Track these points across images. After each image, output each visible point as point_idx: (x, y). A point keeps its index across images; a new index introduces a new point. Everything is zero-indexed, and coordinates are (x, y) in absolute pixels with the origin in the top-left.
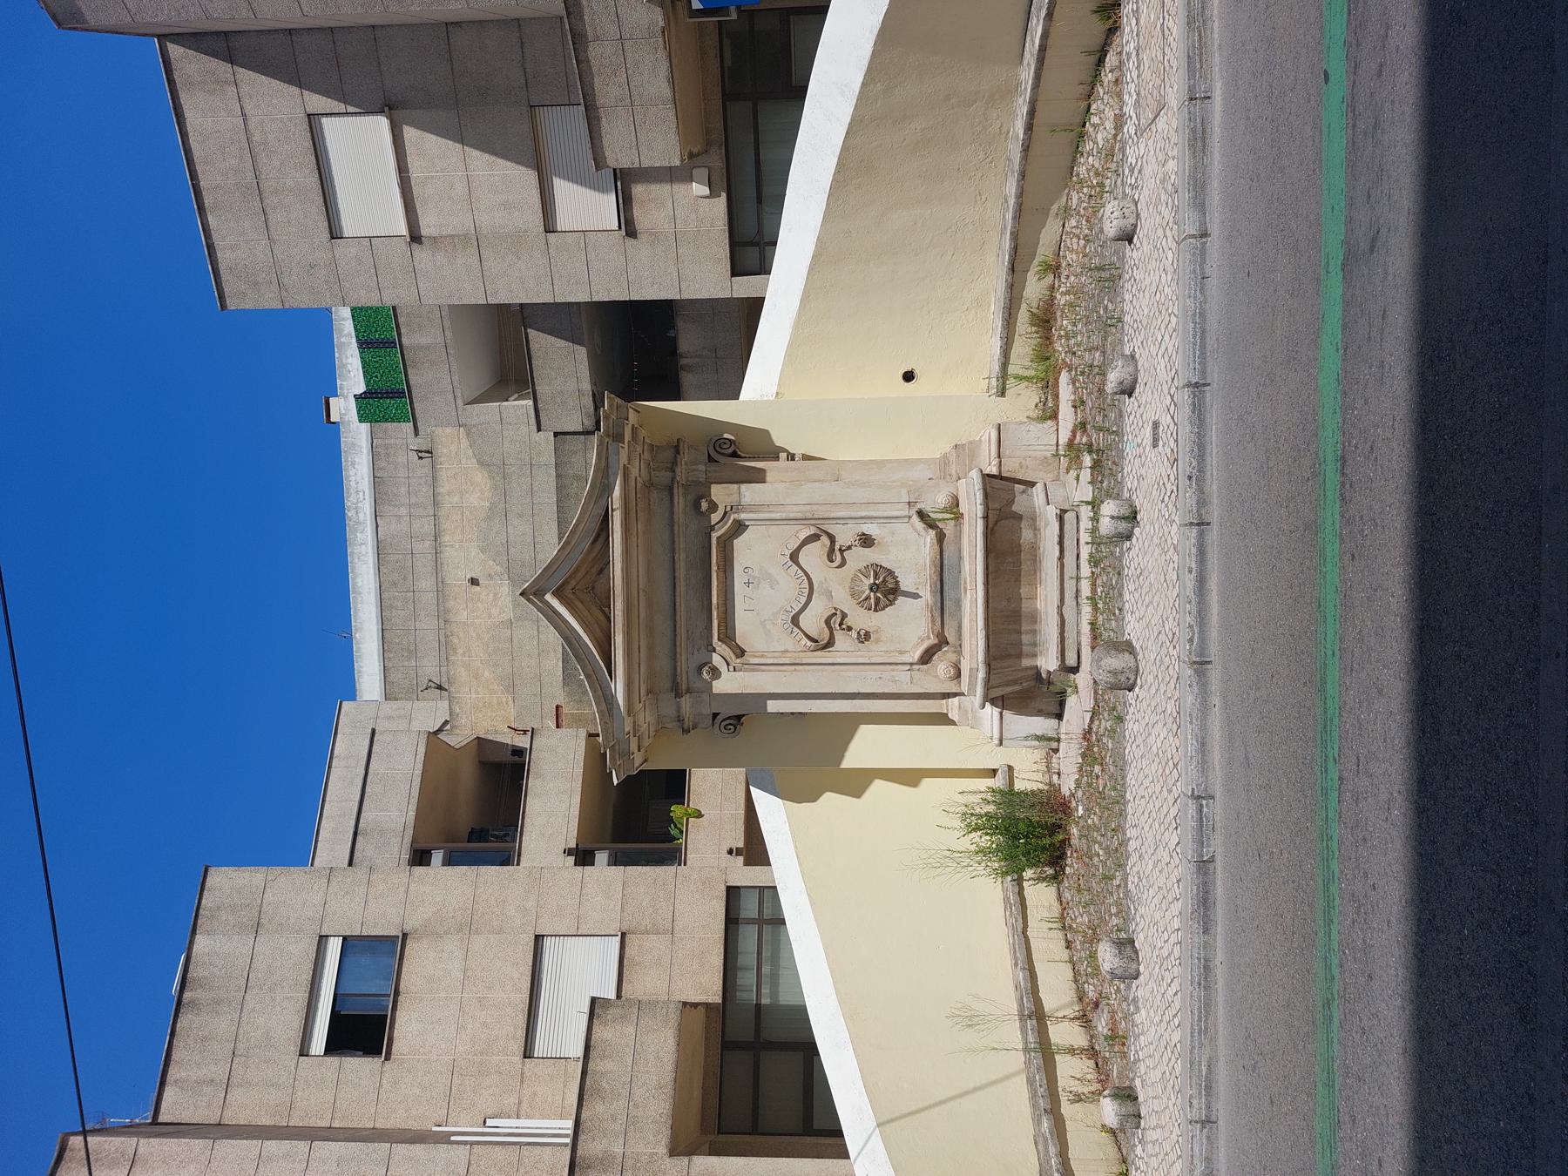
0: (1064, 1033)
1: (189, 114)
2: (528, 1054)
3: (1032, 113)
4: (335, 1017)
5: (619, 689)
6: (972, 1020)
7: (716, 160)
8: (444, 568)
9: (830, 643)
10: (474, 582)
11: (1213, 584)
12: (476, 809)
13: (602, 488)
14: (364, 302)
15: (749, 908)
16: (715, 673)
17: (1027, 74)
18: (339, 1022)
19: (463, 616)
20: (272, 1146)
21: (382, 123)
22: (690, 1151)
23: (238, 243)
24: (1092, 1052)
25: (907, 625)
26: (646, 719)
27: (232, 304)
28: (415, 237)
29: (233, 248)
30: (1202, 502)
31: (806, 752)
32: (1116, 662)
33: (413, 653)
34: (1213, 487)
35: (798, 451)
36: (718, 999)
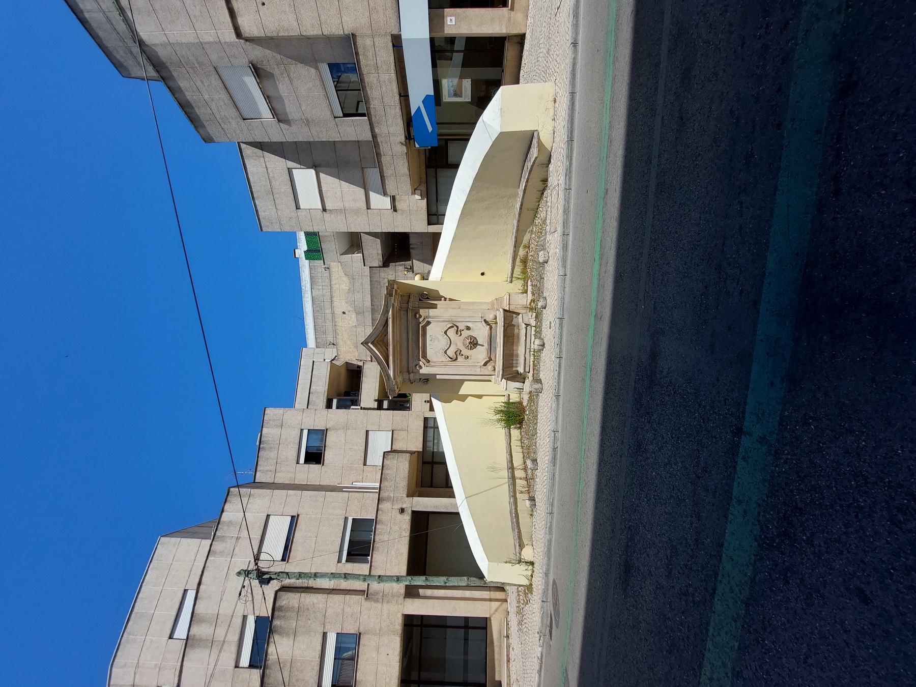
0: (519, 473)
1: (248, 167)
2: (365, 464)
3: (522, 205)
4: (307, 453)
5: (391, 373)
6: (493, 469)
7: (423, 188)
8: (336, 311)
9: (456, 359)
10: (344, 313)
11: (562, 374)
12: (346, 388)
13: (386, 312)
14: (308, 230)
15: (431, 424)
16: (421, 367)
17: (521, 194)
18: (308, 455)
20: (290, 492)
21: (313, 171)
22: (413, 496)
23: (265, 209)
24: (526, 479)
25: (480, 354)
26: (399, 379)
27: (264, 229)
28: (324, 210)
29: (264, 211)
30: (561, 352)
31: (449, 390)
32: (537, 386)
33: (325, 333)
34: (564, 348)
35: (448, 297)
36: (432, 93)
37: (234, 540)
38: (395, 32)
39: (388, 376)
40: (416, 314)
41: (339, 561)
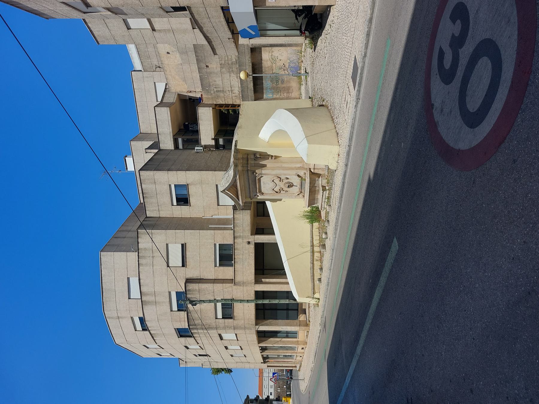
0: (316, 249)
10: (168, 53)
19: (166, 62)
28: (154, 30)
37: (151, 258)
38: (224, 5)
39: (239, 204)
40: (254, 172)
41: (215, 266)
